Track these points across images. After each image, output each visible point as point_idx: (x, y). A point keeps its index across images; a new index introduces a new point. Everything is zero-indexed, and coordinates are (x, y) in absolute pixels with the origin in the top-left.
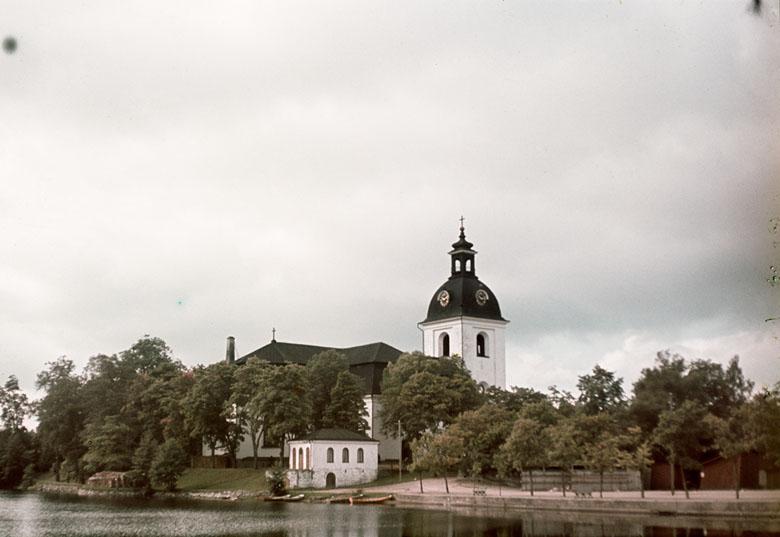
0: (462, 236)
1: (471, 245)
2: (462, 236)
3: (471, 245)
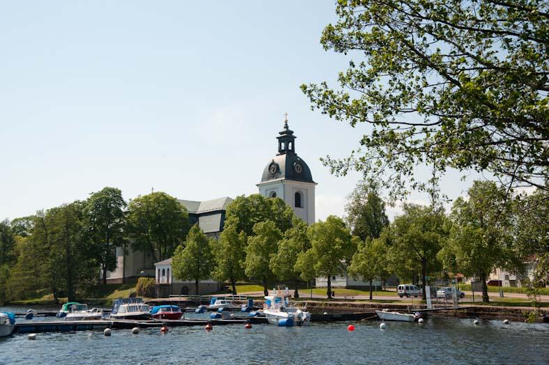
0: (286, 127)
1: (293, 132)
2: (286, 127)
3: (293, 132)
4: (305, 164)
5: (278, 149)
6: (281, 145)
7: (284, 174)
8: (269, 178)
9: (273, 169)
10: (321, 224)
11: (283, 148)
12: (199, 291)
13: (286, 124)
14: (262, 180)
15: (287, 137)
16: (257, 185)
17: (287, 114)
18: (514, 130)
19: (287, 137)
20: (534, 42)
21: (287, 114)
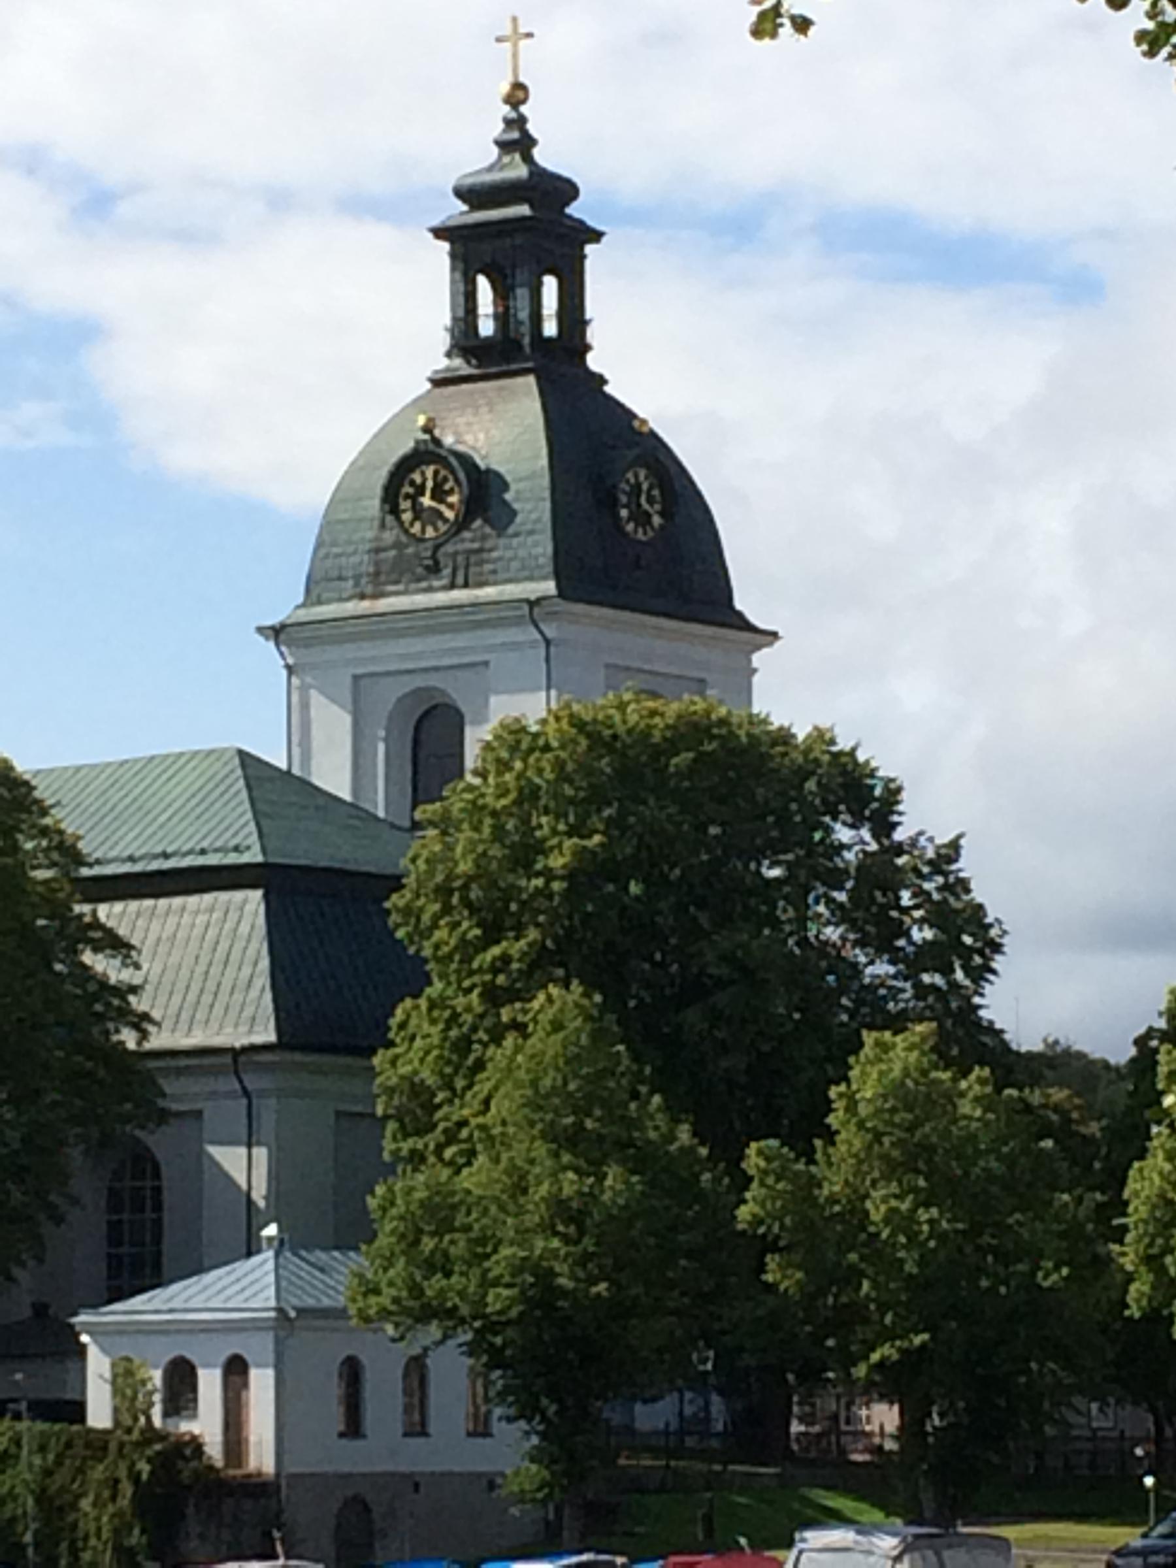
0: (518, 141)
2: (518, 141)
4: (698, 494)
5: (444, 341)
6: (470, 296)
7: (543, 547)
8: (377, 581)
9: (425, 499)
10: (981, 1018)
11: (486, 328)
12: (471, 581)
13: (518, 122)
14: (312, 596)
15: (521, 236)
16: (277, 633)
17: (517, 35)
18: (488, 1079)
19: (521, 236)
20: (629, 850)
21: (517, 35)
